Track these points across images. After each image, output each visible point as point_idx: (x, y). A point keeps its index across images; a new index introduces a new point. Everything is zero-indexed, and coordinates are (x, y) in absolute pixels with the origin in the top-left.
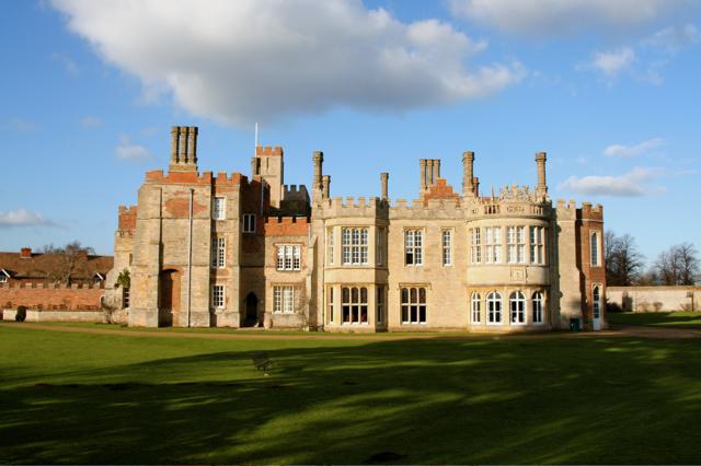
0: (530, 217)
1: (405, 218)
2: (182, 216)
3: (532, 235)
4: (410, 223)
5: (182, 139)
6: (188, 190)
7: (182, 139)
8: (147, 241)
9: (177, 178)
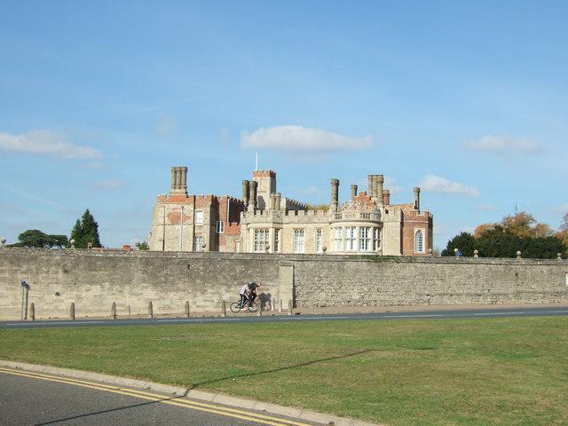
0: (373, 222)
1: (293, 223)
2: (177, 223)
3: (374, 233)
4: (297, 226)
5: (178, 175)
6: (180, 206)
7: (178, 175)
8: (157, 238)
9: (174, 199)
